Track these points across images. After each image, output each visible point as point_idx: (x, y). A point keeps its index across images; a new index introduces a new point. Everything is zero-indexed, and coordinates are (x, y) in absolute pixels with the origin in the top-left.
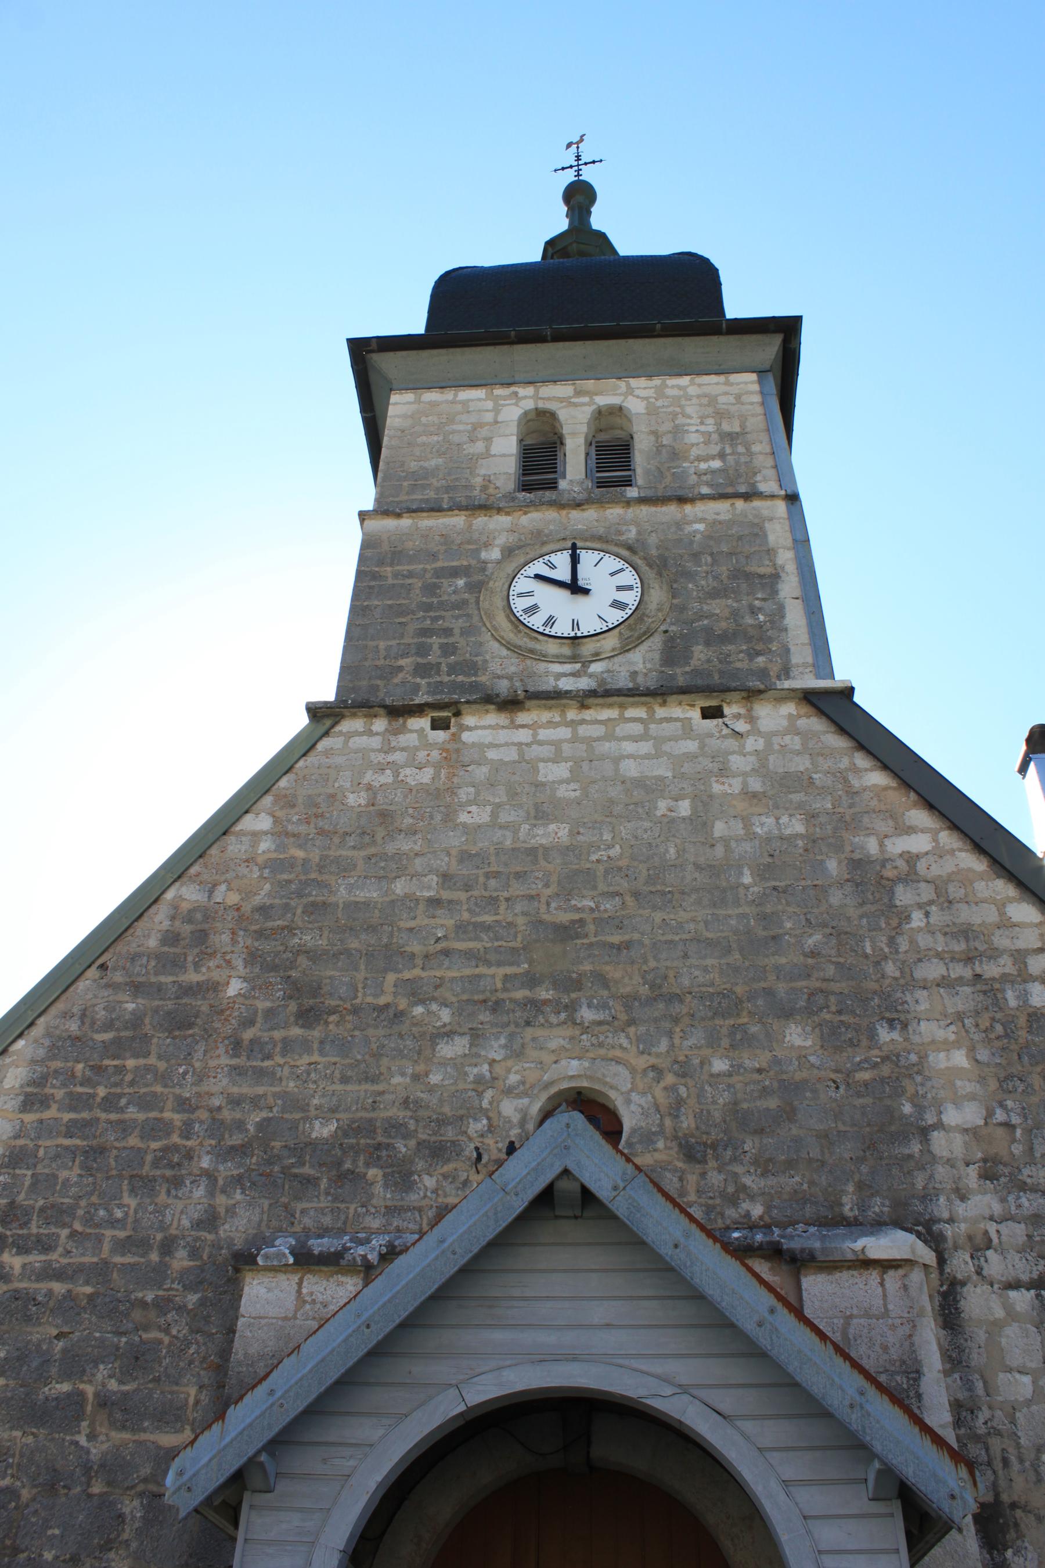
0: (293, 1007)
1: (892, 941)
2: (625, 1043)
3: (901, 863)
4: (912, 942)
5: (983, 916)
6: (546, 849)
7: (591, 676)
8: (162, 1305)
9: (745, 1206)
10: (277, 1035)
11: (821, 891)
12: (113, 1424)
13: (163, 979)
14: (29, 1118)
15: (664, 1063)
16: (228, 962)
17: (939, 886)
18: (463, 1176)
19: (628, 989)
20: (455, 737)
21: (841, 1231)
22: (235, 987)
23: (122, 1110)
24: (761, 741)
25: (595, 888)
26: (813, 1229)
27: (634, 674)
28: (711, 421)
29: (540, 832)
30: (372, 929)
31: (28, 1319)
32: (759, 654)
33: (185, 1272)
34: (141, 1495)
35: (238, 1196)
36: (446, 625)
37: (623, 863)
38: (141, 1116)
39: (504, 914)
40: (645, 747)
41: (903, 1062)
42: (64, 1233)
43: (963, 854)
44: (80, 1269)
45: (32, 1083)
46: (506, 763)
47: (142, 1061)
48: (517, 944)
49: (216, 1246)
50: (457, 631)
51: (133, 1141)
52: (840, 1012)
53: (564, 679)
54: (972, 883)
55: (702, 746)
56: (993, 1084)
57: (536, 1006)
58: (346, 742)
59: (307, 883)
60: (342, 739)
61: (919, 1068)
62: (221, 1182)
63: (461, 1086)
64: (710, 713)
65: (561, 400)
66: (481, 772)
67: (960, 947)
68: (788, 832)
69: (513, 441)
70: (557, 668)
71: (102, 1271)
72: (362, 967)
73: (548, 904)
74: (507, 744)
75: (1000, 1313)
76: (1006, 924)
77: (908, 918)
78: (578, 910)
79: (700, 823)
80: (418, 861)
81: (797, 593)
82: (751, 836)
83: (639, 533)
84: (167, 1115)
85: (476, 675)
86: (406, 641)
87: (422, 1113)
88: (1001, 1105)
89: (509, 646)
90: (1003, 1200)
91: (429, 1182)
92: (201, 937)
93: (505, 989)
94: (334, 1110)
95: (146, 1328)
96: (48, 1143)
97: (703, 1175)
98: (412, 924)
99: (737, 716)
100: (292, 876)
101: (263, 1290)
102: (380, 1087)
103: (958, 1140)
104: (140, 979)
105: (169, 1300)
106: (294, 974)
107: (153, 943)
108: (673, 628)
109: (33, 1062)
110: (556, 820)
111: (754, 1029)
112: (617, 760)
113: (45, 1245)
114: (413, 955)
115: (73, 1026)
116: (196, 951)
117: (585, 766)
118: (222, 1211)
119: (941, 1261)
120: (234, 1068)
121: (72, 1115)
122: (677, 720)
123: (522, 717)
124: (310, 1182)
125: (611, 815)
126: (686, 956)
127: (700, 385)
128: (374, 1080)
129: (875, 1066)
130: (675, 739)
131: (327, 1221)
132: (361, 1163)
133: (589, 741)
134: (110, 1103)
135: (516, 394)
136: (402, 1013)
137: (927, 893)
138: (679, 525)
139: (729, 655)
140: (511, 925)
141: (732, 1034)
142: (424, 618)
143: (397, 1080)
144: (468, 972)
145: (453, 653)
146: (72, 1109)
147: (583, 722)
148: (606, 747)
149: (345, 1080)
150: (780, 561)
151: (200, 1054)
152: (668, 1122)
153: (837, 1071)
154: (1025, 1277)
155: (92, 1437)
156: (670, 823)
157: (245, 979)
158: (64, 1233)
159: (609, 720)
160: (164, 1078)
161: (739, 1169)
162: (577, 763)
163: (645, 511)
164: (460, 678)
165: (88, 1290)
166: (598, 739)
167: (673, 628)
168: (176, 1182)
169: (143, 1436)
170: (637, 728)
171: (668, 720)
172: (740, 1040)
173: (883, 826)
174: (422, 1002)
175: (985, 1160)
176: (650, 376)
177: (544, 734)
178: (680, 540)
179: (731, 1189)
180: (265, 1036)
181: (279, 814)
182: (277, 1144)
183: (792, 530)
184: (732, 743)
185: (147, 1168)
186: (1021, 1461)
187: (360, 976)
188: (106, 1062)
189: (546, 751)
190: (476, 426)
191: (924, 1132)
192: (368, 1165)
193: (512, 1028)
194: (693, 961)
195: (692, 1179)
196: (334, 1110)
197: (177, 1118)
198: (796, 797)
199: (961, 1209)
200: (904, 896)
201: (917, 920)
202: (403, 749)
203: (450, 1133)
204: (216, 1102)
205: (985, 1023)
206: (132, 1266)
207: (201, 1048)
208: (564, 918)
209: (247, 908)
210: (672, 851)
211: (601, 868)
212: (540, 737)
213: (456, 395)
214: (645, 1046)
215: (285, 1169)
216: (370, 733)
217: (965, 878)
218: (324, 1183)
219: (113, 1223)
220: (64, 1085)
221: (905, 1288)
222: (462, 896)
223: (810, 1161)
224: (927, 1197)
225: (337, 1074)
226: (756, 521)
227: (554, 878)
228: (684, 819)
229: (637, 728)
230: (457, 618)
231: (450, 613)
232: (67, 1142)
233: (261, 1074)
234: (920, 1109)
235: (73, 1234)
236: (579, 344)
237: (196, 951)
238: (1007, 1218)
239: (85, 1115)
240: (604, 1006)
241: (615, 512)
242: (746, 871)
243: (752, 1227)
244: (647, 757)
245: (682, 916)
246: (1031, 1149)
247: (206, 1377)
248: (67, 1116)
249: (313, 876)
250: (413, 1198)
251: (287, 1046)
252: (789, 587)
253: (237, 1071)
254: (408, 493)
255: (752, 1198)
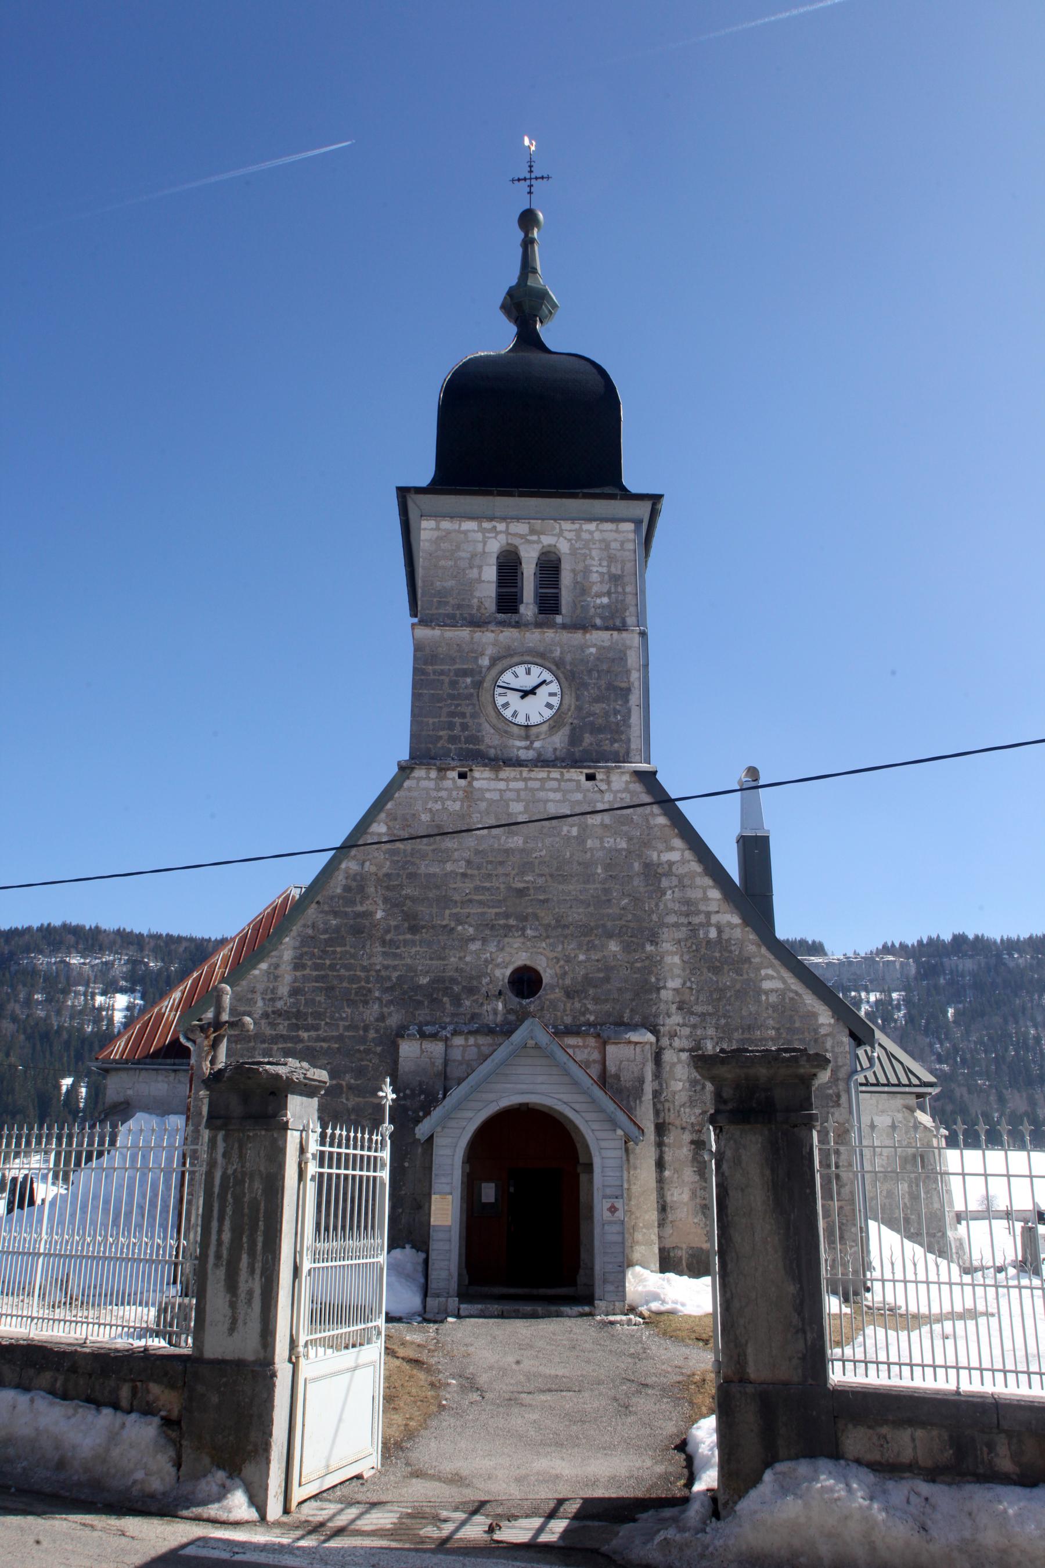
0: (406, 925)
1: (657, 905)
3: (666, 866)
4: (665, 905)
5: (695, 894)
8: (368, 1051)
9: (588, 1016)
10: (401, 937)
11: (631, 878)
13: (347, 909)
14: (298, 974)
15: (560, 956)
17: (681, 878)
18: (481, 1001)
19: (547, 922)
20: (470, 784)
21: (622, 1028)
22: (379, 915)
23: (338, 971)
24: (612, 795)
25: (534, 871)
26: (612, 1027)
27: (555, 749)
30: (438, 887)
32: (616, 741)
33: (374, 1039)
34: (370, 1119)
35: (392, 1008)
36: (463, 710)
37: (547, 859)
38: (347, 974)
40: (558, 796)
41: (654, 960)
42: (323, 1023)
43: (693, 863)
44: (333, 1037)
47: (343, 949)
48: (500, 898)
49: (386, 1028)
50: (468, 715)
51: (345, 984)
52: (631, 937)
53: (521, 750)
54: (694, 877)
55: (585, 796)
56: (688, 972)
57: (509, 928)
58: (418, 783)
59: (406, 862)
60: (415, 781)
61: (660, 962)
62: (384, 1002)
63: (479, 963)
64: (590, 777)
66: (483, 805)
69: (494, 569)
70: (518, 743)
71: (340, 1038)
72: (435, 906)
73: (514, 879)
74: (494, 790)
75: (675, 1060)
76: (706, 899)
77: (665, 894)
79: (581, 840)
80: (456, 853)
83: (561, 653)
84: (358, 973)
85: (478, 744)
86: (442, 719)
88: (689, 980)
89: (494, 727)
90: (684, 1018)
91: (467, 1003)
92: (361, 889)
93: (496, 920)
94: (427, 972)
95: (362, 1060)
96: (309, 985)
97: (573, 1004)
98: (455, 886)
100: (399, 859)
101: (407, 1047)
102: (445, 962)
103: (670, 992)
104: (337, 909)
105: (370, 1050)
107: (339, 891)
108: (575, 721)
109: (295, 948)
111: (597, 942)
113: (316, 1028)
114: (456, 902)
115: (310, 931)
116: (360, 896)
117: (531, 805)
119: (658, 1040)
120: (384, 953)
121: (317, 973)
122: (574, 780)
124: (420, 1003)
126: (571, 907)
128: (443, 959)
129: (643, 961)
131: (428, 1018)
132: (440, 994)
133: (532, 790)
134: (332, 967)
135: (495, 527)
136: (453, 929)
137: (675, 881)
138: (583, 648)
139: (601, 741)
140: (498, 888)
142: (451, 704)
143: (452, 959)
144: (479, 910)
145: (467, 730)
146: (316, 970)
147: (530, 779)
148: (542, 794)
149: (431, 959)
151: (368, 946)
152: (560, 981)
153: (628, 962)
154: (687, 1047)
155: (347, 1099)
156: (568, 838)
158: (323, 1023)
159: (543, 778)
160: (353, 956)
163: (565, 636)
164: (471, 746)
165: (337, 1046)
166: (537, 790)
167: (575, 721)
169: (367, 1100)
170: (554, 784)
172: (591, 947)
173: (661, 846)
174: (461, 924)
175: (679, 1002)
177: (513, 785)
178: (582, 660)
179: (583, 1009)
180: (396, 938)
181: (389, 823)
184: (598, 796)
185: (353, 996)
186: (674, 1110)
188: (328, 949)
190: (473, 556)
191: (658, 989)
192: (443, 996)
193: (498, 938)
194: (574, 910)
195: (569, 1005)
196: (427, 972)
197: (363, 974)
198: (625, 828)
199: (668, 1021)
200: (665, 883)
202: (446, 790)
203: (475, 983)
204: (378, 967)
205: (689, 944)
206: (354, 1036)
207: (368, 943)
208: (520, 885)
209: (380, 874)
210: (568, 854)
211: (537, 861)
212: (510, 787)
213: (460, 525)
214: (553, 946)
215: (410, 997)
216: (428, 778)
217: (692, 875)
218: (426, 1003)
219: (342, 1019)
220: (311, 959)
221: (643, 1051)
222: (476, 872)
223: (614, 999)
224: (656, 1016)
225: (428, 956)
226: (622, 649)
228: (574, 837)
229: (554, 784)
230: (468, 705)
231: (464, 702)
232: (317, 984)
234: (658, 980)
235: (327, 1023)
236: (534, 499)
237: (360, 896)
238: (684, 1025)
239: (322, 973)
240: (537, 929)
241: (550, 634)
242: (599, 867)
245: (571, 887)
246: (698, 999)
248: (315, 973)
249: (408, 859)
251: (406, 943)
252: (634, 699)
254: (436, 608)
255: (590, 1013)
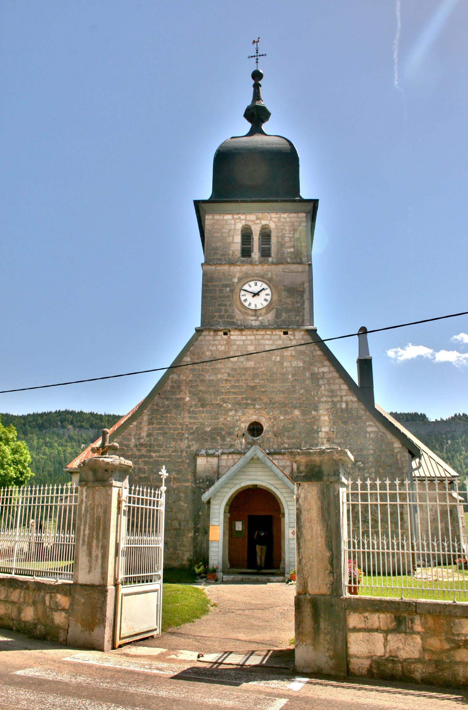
0: (200, 403)
1: (317, 392)
2: (264, 412)
3: (321, 374)
4: (321, 393)
6: (249, 368)
7: (259, 321)
8: (183, 462)
10: (197, 409)
11: (304, 380)
12: (177, 482)
14: (150, 427)
15: (272, 417)
16: (185, 393)
17: (328, 380)
20: (229, 338)
22: (187, 399)
24: (296, 341)
27: (269, 321)
28: (292, 232)
29: (248, 363)
30: (214, 386)
31: (158, 465)
32: (297, 316)
33: (185, 456)
35: (193, 442)
37: (265, 372)
38: (173, 426)
39: (241, 383)
42: (162, 449)
44: (166, 456)
45: (149, 419)
46: (240, 345)
48: (244, 390)
49: (191, 451)
51: (172, 431)
52: (305, 408)
56: (332, 423)
57: (247, 404)
61: (319, 419)
64: (285, 333)
65: (252, 221)
66: (235, 347)
67: (330, 394)
68: (299, 366)
71: (170, 456)
74: (241, 340)
76: (340, 389)
77: (321, 387)
78: (256, 383)
79: (281, 363)
80: (223, 370)
81: (308, 297)
82: (291, 366)
83: (271, 275)
84: (178, 426)
87: (226, 426)
91: (228, 440)
94: (210, 425)
95: (180, 466)
97: (278, 439)
98: (222, 385)
99: (291, 334)
103: (324, 434)
105: (183, 461)
106: (199, 396)
107: (169, 388)
108: (278, 307)
109: (149, 415)
110: (251, 361)
111: (289, 410)
112: (265, 345)
113: (159, 451)
114: (223, 393)
118: (191, 445)
123: (244, 333)
124: (207, 439)
125: (263, 360)
126: (277, 394)
127: (290, 217)
128: (217, 419)
129: (311, 419)
130: (277, 340)
131: (210, 447)
133: (258, 340)
135: (240, 217)
137: (326, 381)
140: (242, 386)
141: (284, 412)
144: (234, 396)
146: (159, 425)
147: (257, 334)
148: (262, 342)
149: (211, 419)
150: (305, 287)
152: (272, 429)
155: (173, 484)
156: (275, 362)
157: (189, 397)
158: (162, 449)
159: (263, 334)
161: (284, 438)
162: (256, 345)
164: (229, 320)
165: (168, 459)
166: (260, 339)
168: (181, 440)
171: (276, 335)
172: (286, 413)
173: (319, 365)
174: (225, 403)
176: (277, 213)
177: (249, 337)
180: (195, 410)
182: (200, 432)
183: (309, 276)
187: (213, 397)
188: (164, 415)
189: (249, 342)
191: (318, 432)
195: (276, 440)
196: (210, 425)
197: (180, 427)
201: (323, 387)
202: (218, 340)
203: (232, 430)
204: (187, 423)
208: (253, 384)
209: (188, 380)
211: (260, 373)
213: (224, 217)
214: (268, 413)
216: (210, 335)
218: (209, 439)
219: (171, 447)
220: (156, 420)
222: (232, 379)
227: (251, 375)
229: (268, 337)
230: (227, 301)
231: (226, 299)
232: (159, 432)
233: (195, 418)
234: (318, 428)
235: (163, 450)
239: (161, 426)
240: (260, 405)
241: (266, 267)
242: (290, 375)
243: (286, 449)
244: (271, 345)
245: (276, 385)
247: (192, 474)
248: (158, 426)
249: (201, 373)
250: (226, 443)
253: (190, 417)
255: (286, 444)
